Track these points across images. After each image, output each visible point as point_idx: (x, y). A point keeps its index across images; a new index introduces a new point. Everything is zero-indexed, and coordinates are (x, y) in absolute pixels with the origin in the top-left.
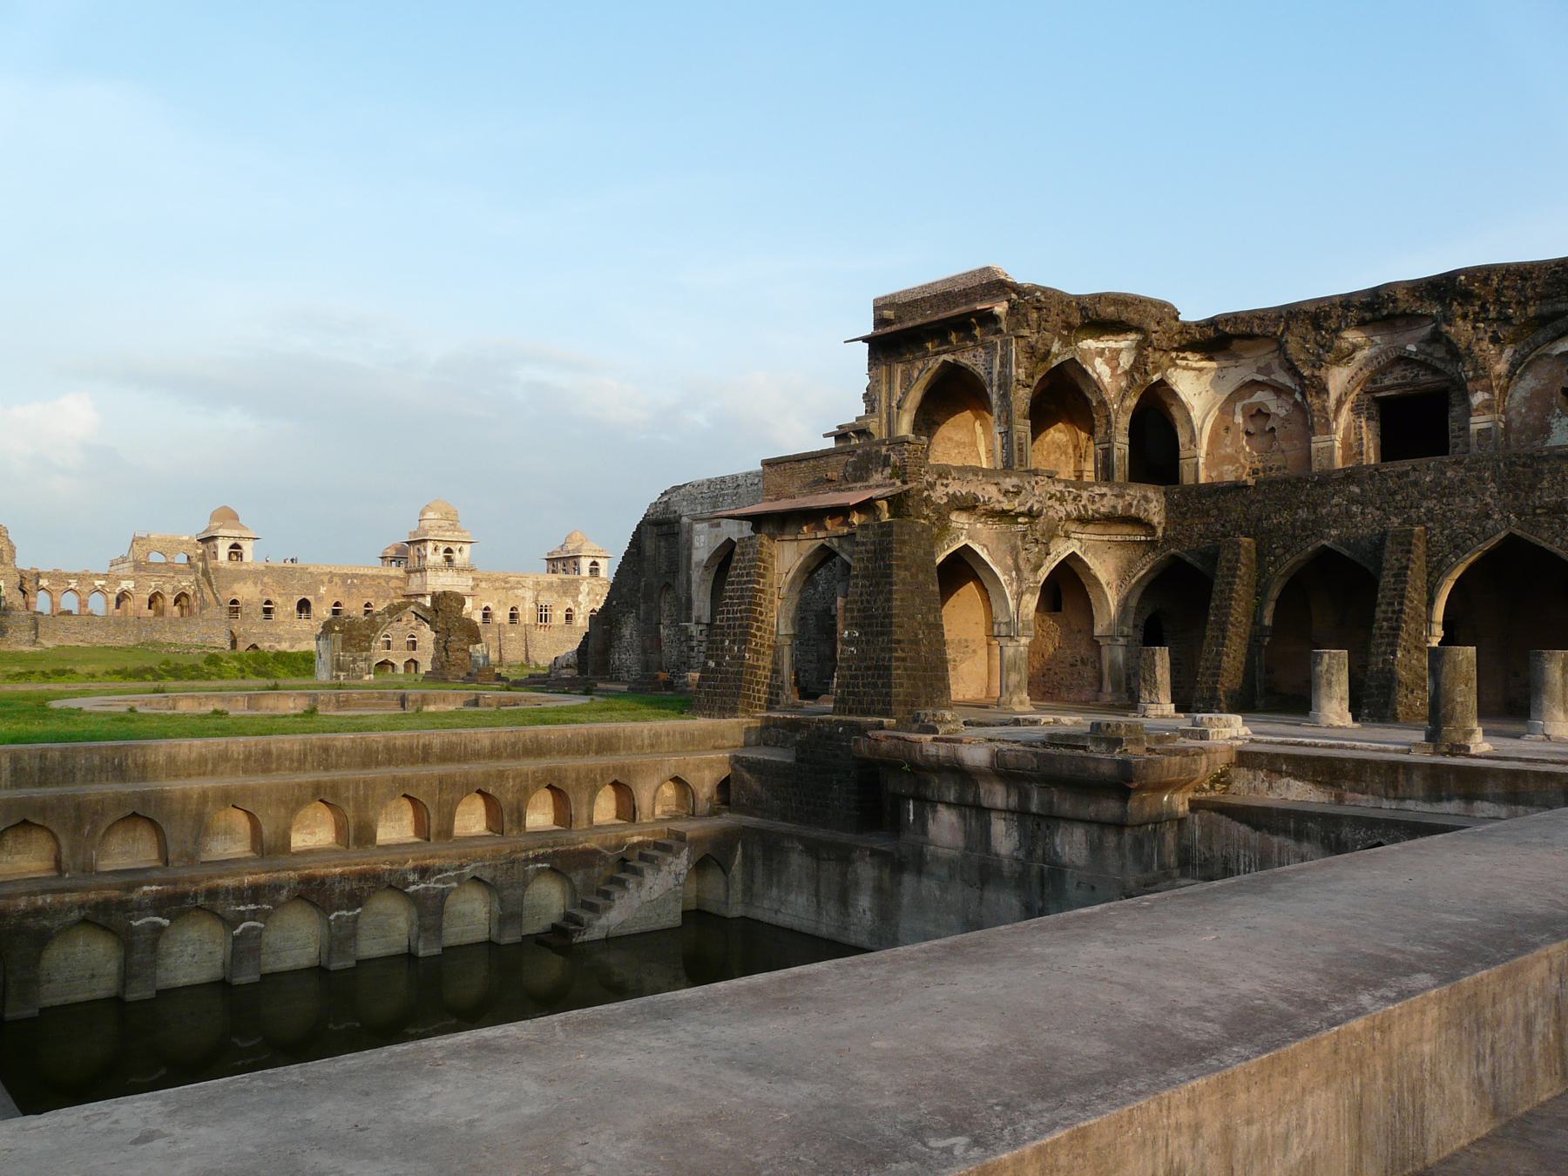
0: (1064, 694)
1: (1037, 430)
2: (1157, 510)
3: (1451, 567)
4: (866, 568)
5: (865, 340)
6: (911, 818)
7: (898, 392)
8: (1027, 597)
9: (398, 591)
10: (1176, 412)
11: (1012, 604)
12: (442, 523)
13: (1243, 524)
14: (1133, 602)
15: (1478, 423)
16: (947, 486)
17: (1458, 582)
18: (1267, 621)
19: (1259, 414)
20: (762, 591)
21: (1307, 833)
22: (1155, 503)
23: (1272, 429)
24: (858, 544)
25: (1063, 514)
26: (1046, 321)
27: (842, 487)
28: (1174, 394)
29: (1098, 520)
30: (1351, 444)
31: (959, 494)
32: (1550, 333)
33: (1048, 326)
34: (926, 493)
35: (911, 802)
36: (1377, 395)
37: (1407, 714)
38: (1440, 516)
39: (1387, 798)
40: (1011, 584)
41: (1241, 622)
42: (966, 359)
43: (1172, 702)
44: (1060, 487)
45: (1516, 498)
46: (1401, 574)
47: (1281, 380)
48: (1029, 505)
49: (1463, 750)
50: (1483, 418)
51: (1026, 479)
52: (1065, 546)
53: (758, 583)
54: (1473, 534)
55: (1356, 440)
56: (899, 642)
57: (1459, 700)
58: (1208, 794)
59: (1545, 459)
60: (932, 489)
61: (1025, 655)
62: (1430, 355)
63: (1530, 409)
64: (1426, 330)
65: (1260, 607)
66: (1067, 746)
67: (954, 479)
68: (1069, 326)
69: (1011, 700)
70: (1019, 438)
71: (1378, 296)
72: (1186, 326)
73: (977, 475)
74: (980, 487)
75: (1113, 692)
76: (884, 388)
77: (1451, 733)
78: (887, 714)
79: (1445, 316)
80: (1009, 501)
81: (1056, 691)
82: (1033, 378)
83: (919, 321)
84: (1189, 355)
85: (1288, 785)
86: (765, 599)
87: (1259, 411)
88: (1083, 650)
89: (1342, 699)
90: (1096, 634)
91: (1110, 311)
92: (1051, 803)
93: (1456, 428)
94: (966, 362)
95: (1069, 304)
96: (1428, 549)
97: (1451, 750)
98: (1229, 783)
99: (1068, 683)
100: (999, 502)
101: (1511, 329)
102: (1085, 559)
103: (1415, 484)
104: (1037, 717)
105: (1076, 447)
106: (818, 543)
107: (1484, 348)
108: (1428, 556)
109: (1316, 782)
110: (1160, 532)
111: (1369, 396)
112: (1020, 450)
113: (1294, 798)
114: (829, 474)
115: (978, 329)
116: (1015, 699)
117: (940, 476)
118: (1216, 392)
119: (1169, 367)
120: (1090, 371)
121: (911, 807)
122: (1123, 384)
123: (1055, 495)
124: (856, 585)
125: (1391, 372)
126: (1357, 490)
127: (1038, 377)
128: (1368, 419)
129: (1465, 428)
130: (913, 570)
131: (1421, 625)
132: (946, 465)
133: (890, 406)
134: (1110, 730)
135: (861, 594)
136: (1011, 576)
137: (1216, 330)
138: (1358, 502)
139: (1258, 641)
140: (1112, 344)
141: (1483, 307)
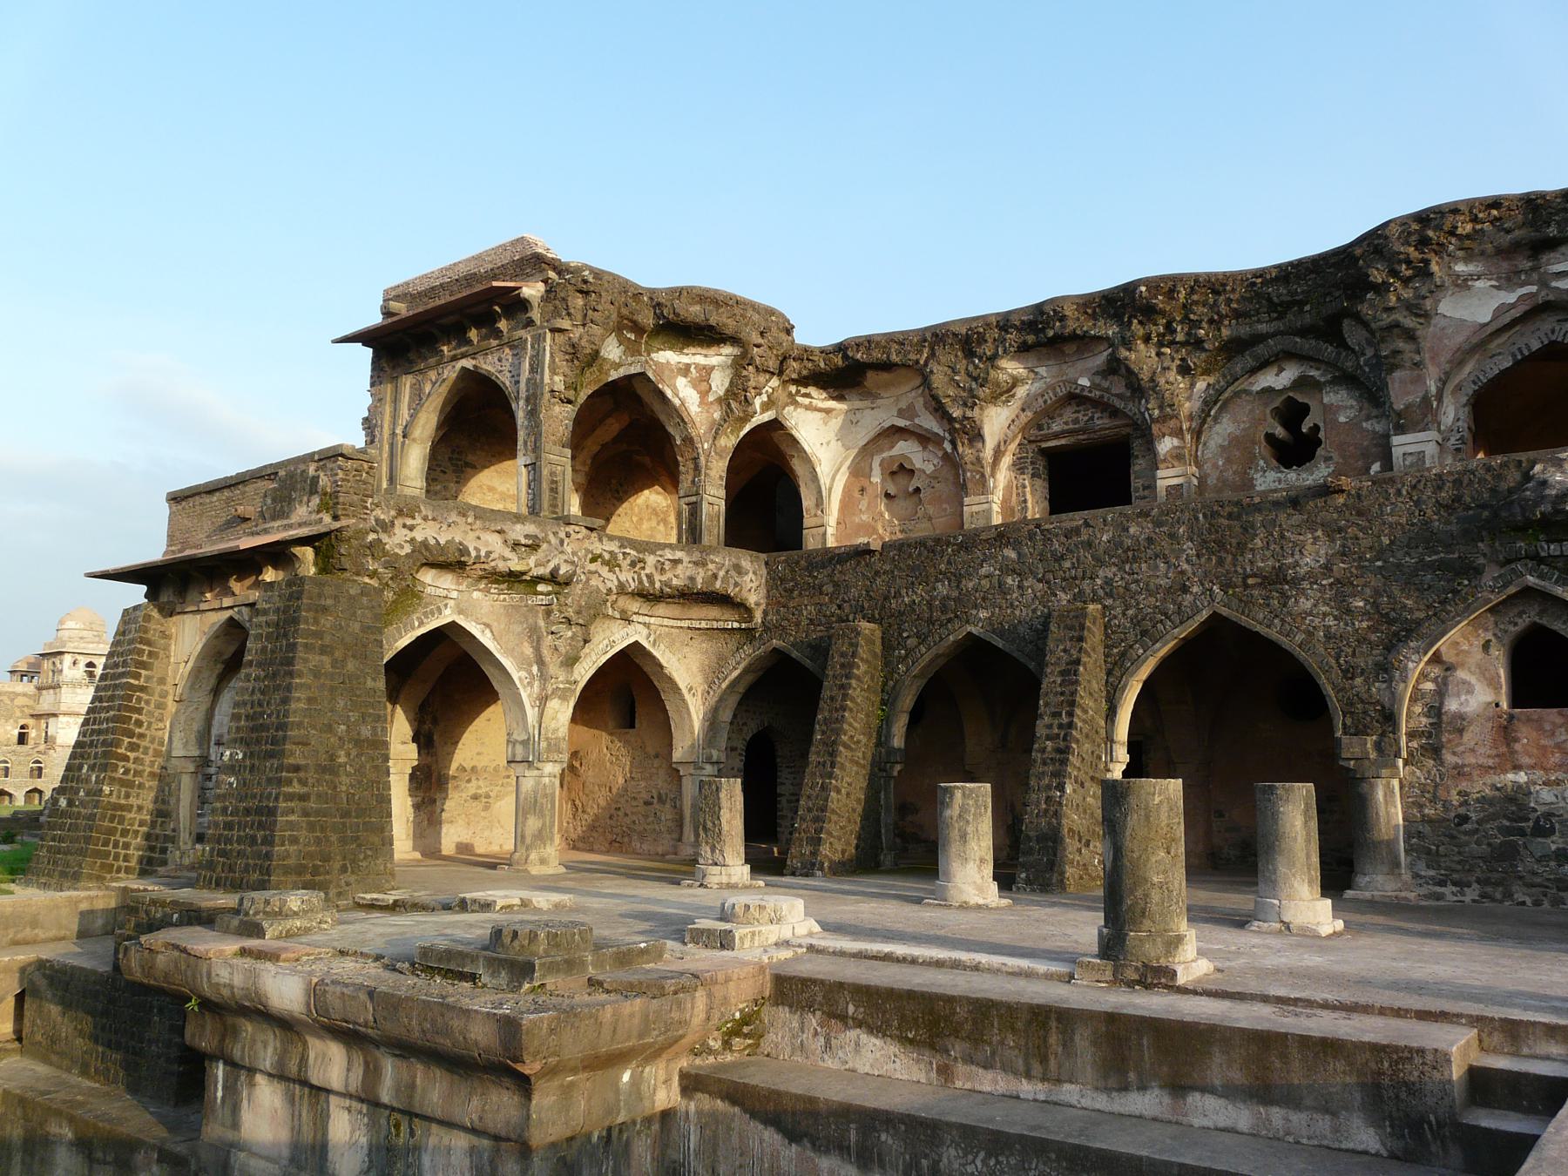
0: (636, 844)
2: (754, 585)
3: (1138, 662)
4: (264, 649)
5: (363, 337)
6: (220, 1094)
8: (553, 704)
9: (25, 709)
10: (797, 466)
11: (531, 714)
12: (85, 633)
13: (866, 605)
14: (726, 716)
15: (1167, 478)
16: (411, 528)
17: (1147, 685)
18: (898, 742)
19: (902, 470)
20: (142, 689)
21: (879, 1155)
22: (751, 575)
23: (917, 490)
25: (613, 585)
26: (595, 310)
30: (1012, 510)
31: (432, 542)
32: (1250, 362)
34: (371, 537)
35: (221, 1066)
36: (1044, 445)
37: (1081, 878)
38: (1121, 590)
39: (1028, 1076)
40: (530, 684)
41: (859, 742)
43: (747, 861)
44: (613, 546)
45: (1221, 562)
46: (1070, 672)
48: (551, 566)
49: (1158, 977)
50: (1171, 472)
53: (137, 676)
54: (1166, 614)
56: (297, 769)
57: (1155, 880)
58: (720, 1059)
59: (1257, 508)
60: (385, 531)
62: (1107, 390)
63: (1228, 461)
64: (1100, 359)
67: (425, 519)
68: (638, 329)
69: (528, 856)
70: (552, 474)
71: (1042, 313)
72: (806, 353)
73: (464, 515)
74: (472, 535)
76: (388, 409)
77: (1143, 945)
79: (1123, 338)
81: (626, 839)
84: (812, 390)
85: (857, 1044)
86: (147, 702)
87: (901, 466)
88: (661, 782)
89: (982, 861)
90: (674, 760)
91: (694, 312)
92: (412, 1086)
93: (1139, 485)
96: (1107, 636)
97: (1144, 976)
98: (758, 1036)
100: (505, 559)
101: (1203, 355)
103: (1089, 545)
107: (1171, 379)
108: (1106, 646)
109: (903, 1040)
110: (758, 617)
111: (1034, 446)
112: (554, 491)
113: (867, 1069)
116: (533, 856)
117: (400, 513)
119: (787, 405)
120: (669, 394)
121: (220, 1074)
122: (717, 415)
123: (600, 556)
126: (1013, 555)
128: (1033, 476)
129: (1151, 487)
130: (337, 654)
131: (1099, 746)
133: (393, 434)
134: (516, 943)
136: (530, 673)
137: (845, 357)
138: (1014, 571)
139: (885, 771)
140: (700, 360)
141: (1169, 328)
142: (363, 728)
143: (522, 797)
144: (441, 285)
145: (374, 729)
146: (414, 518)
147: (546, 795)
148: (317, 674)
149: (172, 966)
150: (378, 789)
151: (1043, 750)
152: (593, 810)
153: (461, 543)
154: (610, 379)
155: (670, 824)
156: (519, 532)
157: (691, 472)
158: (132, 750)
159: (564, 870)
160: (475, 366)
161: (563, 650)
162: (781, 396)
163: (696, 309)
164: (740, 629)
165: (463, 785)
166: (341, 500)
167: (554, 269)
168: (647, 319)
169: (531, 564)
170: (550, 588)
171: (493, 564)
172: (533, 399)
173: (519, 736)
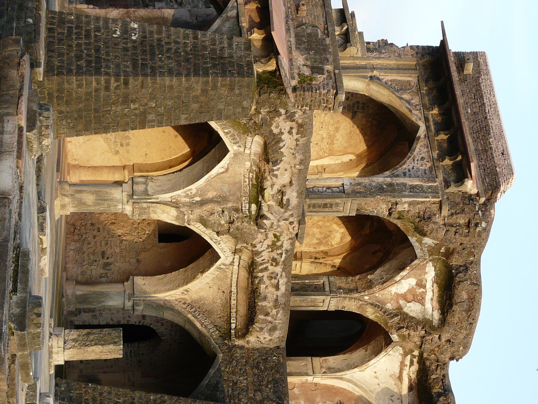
1: (347, 221)
2: (262, 339)
4: (205, 48)
5: (444, 43)
8: (173, 212)
10: (359, 353)
11: (166, 197)
14: (168, 316)
22: (269, 338)
24: (230, 39)
25: (259, 248)
26: (456, 233)
27: (290, 22)
28: (377, 353)
29: (252, 282)
31: (281, 145)
33: (451, 234)
34: (283, 111)
40: (187, 196)
43: (66, 362)
44: (287, 245)
48: (269, 215)
51: (296, 212)
52: (226, 249)
56: (126, 83)
60: (287, 118)
61: (113, 210)
66: (16, 272)
67: (297, 140)
68: (449, 254)
70: (337, 205)
72: (445, 365)
73: (300, 163)
74: (288, 167)
75: (76, 295)
76: (392, 63)
78: (49, 71)
80: (273, 196)
81: (76, 237)
82: (399, 218)
83: (461, 101)
84: (415, 367)
90: (136, 278)
94: (417, 150)
95: (472, 254)
99: (85, 250)
100: (272, 186)
104: (48, 230)
105: (326, 254)
110: (239, 342)
112: (325, 206)
114: (305, 8)
115: (451, 163)
116: (67, 200)
117: (300, 126)
118: (378, 394)
119: (404, 348)
122: (389, 306)
123: (278, 240)
124: (186, 37)
127: (399, 223)
130: (202, 98)
132: (311, 133)
133: (373, 68)
134: (34, 316)
135: (177, 43)
136: (195, 196)
137: (439, 395)
140: (429, 295)
142: (154, 115)
144: (484, 104)
145: (153, 121)
146: (297, 134)
149: (11, 83)
150: (113, 126)
153: (281, 161)
154: (409, 238)
157: (347, 286)
159: (57, 218)
160: (419, 137)
161: (211, 218)
163: (464, 295)
164: (231, 329)
166: (307, 93)
167: (488, 200)
168: (455, 261)
170: (253, 213)
171: (269, 178)
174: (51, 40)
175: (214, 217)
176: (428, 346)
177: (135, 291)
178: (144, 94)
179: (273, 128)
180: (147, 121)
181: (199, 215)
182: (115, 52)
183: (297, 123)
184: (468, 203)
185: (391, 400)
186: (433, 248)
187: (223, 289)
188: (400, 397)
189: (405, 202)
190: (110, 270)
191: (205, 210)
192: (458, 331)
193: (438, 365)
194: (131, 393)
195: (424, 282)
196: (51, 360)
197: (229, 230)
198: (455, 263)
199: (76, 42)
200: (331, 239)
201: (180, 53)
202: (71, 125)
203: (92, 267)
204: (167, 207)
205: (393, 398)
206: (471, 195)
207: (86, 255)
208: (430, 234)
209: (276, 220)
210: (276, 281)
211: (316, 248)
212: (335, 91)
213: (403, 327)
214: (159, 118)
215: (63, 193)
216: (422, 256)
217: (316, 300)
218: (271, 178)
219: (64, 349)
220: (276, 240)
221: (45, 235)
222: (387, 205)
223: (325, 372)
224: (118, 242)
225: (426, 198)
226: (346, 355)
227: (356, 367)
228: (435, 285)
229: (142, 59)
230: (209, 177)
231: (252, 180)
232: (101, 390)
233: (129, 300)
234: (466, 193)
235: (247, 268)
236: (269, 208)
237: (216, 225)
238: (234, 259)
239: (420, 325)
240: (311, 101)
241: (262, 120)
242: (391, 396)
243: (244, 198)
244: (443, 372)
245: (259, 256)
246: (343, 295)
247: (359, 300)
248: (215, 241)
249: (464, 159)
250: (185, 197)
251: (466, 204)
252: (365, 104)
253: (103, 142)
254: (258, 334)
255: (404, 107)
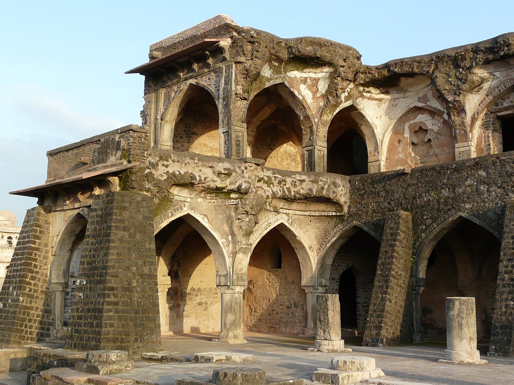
2: (343, 192)
4: (95, 229)
5: (140, 70)
7: (162, 108)
8: (240, 256)
11: (229, 261)
12: (7, 222)
13: (403, 202)
14: (329, 261)
16: (167, 166)
18: (422, 275)
19: (421, 130)
20: (37, 249)
22: (341, 187)
23: (429, 140)
25: (270, 193)
26: (257, 51)
28: (363, 117)
31: (177, 173)
34: (147, 171)
36: (499, 114)
41: (401, 275)
42: (203, 82)
43: (342, 338)
44: (269, 174)
47: (434, 105)
48: (238, 184)
52: (275, 218)
53: (34, 243)
55: (486, 146)
56: (112, 289)
65: (416, 264)
67: (174, 161)
68: (279, 60)
70: (237, 136)
71: (497, 43)
74: (197, 169)
76: (153, 106)
80: (222, 181)
81: (278, 326)
84: (371, 89)
86: (39, 256)
87: (420, 128)
88: (296, 297)
89: (471, 339)
90: (302, 285)
91: (309, 50)
94: (204, 83)
99: (286, 320)
100: (214, 181)
102: (292, 229)
106: (76, 212)
110: (346, 209)
111: (493, 115)
112: (238, 145)
116: (231, 334)
117: (161, 158)
119: (358, 97)
120: (296, 93)
122: (322, 104)
123: (263, 179)
125: (508, 98)
126: (484, 174)
128: (493, 131)
133: (156, 119)
136: (227, 240)
137: (389, 71)
138: (484, 182)
139: (415, 290)
140: (312, 75)
142: (144, 268)
143: (224, 304)
145: (150, 269)
146: (168, 161)
147: (237, 303)
148: (121, 241)
150: (153, 300)
151: (503, 279)
152: (260, 311)
153: (192, 173)
154: (266, 87)
155: (300, 318)
156: (221, 167)
157: (309, 134)
158: (32, 280)
159: (246, 342)
160: (196, 83)
161: (244, 228)
162: (355, 93)
163: (309, 48)
164: (336, 216)
165: (194, 297)
166: (132, 153)
168: (284, 55)
169: (227, 184)
170: (237, 196)
171: (208, 184)
172: (227, 98)
173: (222, 272)
174: (80, 346)
175: (243, 226)
176: (350, 75)
177: (311, 285)
178: (124, 275)
179: (163, 179)
180: (150, 273)
181: (243, 237)
182: (91, 297)
183: (159, 161)
184: (236, 44)
185: (396, 106)
186: (274, 70)
187: (308, 221)
188: (393, 100)
189: (235, 88)
190: (298, 302)
191: (238, 232)
192: (337, 54)
193: (369, 73)
194: (375, 288)
195: (302, 78)
196: (339, 351)
197: (254, 215)
198: (286, 56)
199: (83, 327)
200: (291, 152)
201: (96, 247)
202: (149, 332)
203: (297, 315)
204: (236, 260)
205: (395, 105)
206: (232, 43)
207: (289, 320)
208: (258, 69)
209: (242, 179)
210: (297, 181)
211: (299, 163)
212: (131, 132)
213: (336, 93)
214: (147, 264)
215: (226, 337)
216: (282, 79)
217: (318, 156)
218: (208, 182)
219: (330, 340)
220: (262, 181)
221: (213, 358)
222: (237, 101)
223: (378, 153)
224: (281, 297)
225: (232, 73)
226: (366, 139)
227: (373, 131)
228: (304, 71)
229: (97, 276)
230: (212, 229)
231: (213, 197)
232: (372, 311)
233: (318, 289)
234: (230, 46)
235: (290, 203)
236: (232, 184)
237: (249, 224)
238: (284, 213)
239: (334, 81)
240: (139, 149)
241: (154, 187)
242: (393, 106)
243: (227, 203)
244: (374, 69)
245: (277, 193)
246: (315, 137)
247: (318, 125)
248: (268, 226)
249: (208, 49)
250: (229, 247)
251: (237, 45)
252: (186, 126)
253: (214, 306)
254: (339, 195)
255: (179, 96)
